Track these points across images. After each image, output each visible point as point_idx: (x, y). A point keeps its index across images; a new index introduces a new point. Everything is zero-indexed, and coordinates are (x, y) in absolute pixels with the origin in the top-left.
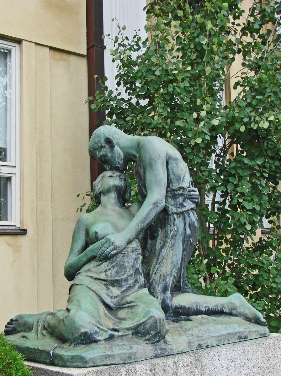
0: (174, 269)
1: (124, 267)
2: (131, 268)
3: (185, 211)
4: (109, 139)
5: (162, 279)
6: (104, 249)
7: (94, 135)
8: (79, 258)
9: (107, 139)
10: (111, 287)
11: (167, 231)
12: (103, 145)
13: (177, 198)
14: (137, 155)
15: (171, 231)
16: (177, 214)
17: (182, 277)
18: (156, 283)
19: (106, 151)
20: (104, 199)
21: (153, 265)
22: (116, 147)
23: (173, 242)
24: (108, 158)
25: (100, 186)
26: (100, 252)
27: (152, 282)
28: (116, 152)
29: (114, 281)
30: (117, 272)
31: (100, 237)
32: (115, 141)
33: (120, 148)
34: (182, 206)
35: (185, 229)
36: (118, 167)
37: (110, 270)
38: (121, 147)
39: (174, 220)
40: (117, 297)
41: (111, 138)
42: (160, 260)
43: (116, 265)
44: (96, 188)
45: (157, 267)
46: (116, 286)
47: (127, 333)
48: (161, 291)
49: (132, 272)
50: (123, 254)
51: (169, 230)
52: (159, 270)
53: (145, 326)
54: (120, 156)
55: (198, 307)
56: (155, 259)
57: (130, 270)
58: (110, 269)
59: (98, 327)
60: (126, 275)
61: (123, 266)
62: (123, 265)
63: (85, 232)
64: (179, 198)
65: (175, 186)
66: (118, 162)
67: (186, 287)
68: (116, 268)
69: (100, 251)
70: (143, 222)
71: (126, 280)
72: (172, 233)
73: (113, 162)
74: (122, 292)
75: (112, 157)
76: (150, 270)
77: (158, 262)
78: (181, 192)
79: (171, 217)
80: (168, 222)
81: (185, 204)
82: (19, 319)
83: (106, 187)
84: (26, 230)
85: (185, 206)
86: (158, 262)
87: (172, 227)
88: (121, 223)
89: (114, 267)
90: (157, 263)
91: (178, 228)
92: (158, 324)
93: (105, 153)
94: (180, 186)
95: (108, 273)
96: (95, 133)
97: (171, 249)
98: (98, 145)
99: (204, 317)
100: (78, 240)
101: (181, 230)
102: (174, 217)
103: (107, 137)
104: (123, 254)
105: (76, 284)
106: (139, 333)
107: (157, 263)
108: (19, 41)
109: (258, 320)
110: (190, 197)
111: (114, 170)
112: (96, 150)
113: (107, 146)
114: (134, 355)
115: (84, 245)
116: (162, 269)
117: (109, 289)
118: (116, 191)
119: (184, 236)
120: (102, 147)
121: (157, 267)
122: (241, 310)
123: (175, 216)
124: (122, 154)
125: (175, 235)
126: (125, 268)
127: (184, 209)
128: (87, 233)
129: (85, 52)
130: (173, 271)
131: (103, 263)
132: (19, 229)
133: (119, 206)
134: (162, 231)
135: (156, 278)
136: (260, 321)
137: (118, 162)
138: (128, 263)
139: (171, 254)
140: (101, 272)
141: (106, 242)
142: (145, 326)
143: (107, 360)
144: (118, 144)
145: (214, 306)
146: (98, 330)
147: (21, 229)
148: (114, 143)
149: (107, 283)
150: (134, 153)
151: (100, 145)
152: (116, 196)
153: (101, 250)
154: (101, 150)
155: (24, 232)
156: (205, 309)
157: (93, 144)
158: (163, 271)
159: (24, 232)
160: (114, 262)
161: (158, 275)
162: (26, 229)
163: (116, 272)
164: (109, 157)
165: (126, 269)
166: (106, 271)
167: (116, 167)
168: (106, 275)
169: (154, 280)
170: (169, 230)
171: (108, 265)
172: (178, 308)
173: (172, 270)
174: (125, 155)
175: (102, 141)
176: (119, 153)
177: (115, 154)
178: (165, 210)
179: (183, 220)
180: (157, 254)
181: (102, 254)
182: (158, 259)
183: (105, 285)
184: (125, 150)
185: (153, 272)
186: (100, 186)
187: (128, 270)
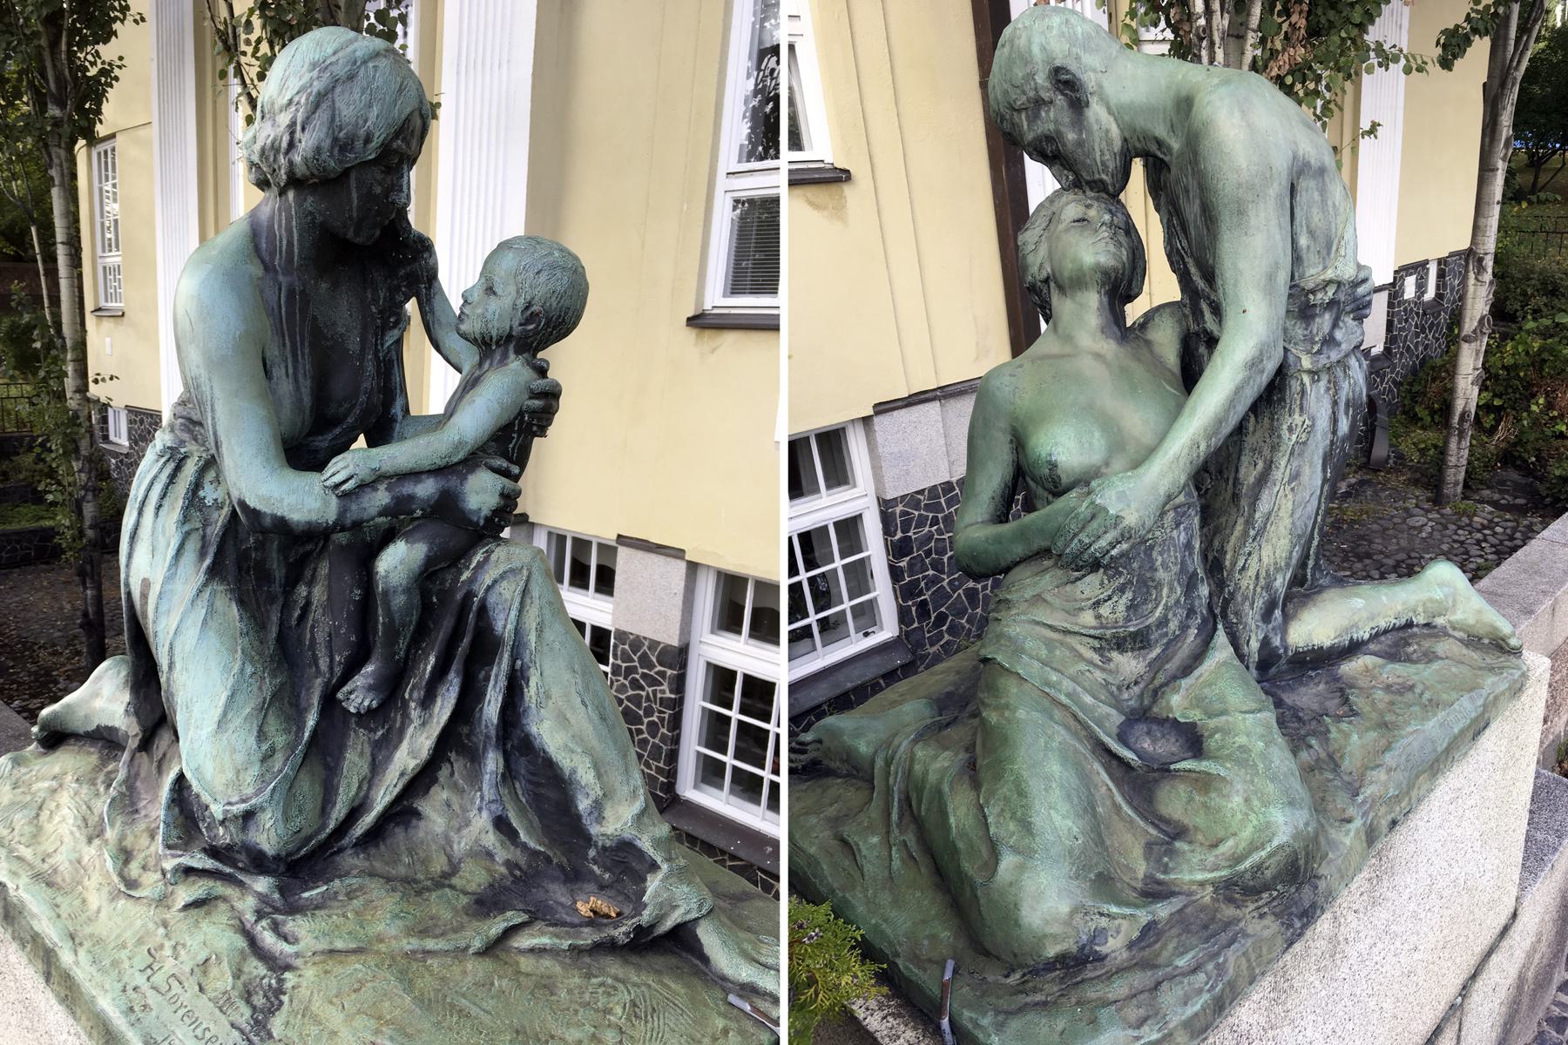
4: (1068, 72)
5: (1262, 582)
6: (1087, 541)
7: (1006, 50)
8: (998, 539)
9: (1057, 70)
10: (1115, 655)
11: (1279, 428)
12: (1045, 95)
13: (1313, 316)
14: (1175, 145)
15: (1290, 429)
17: (1312, 557)
18: (1245, 598)
19: (1056, 122)
20: (1063, 306)
21: (1233, 539)
22: (1093, 101)
23: (1295, 464)
24: (1064, 145)
25: (1043, 250)
26: (1075, 544)
27: (1232, 594)
28: (1096, 127)
29: (1124, 638)
30: (1132, 607)
31: (1065, 480)
32: (1089, 80)
34: (1330, 341)
35: (1335, 421)
36: (1102, 181)
38: (1112, 103)
39: (1303, 392)
40: (1136, 683)
41: (1073, 67)
44: (1030, 259)
45: (1247, 550)
46: (1133, 650)
48: (1258, 617)
51: (1285, 427)
52: (1255, 557)
54: (1110, 143)
56: (1241, 521)
57: (1171, 589)
58: (1110, 598)
60: (1160, 608)
63: (1009, 438)
64: (1321, 315)
66: (1103, 163)
68: (1129, 595)
70: (1215, 433)
72: (1294, 437)
73: (1084, 163)
74: (1150, 665)
75: (1080, 143)
76: (1223, 552)
77: (1252, 533)
78: (1330, 294)
79: (1293, 382)
80: (1283, 399)
82: (825, 739)
86: (1252, 533)
87: (1296, 416)
88: (1138, 419)
89: (1122, 590)
90: (1245, 534)
91: (1313, 419)
92: (1302, 862)
93: (1052, 127)
94: (1330, 274)
95: (1105, 610)
97: (1288, 488)
98: (1024, 93)
100: (990, 464)
101: (1323, 423)
102: (1302, 384)
103: (1058, 63)
107: (1245, 534)
108: (700, 322)
112: (1019, 111)
113: (1060, 100)
115: (1009, 478)
116: (1264, 553)
117: (1110, 660)
118: (1103, 285)
120: (1039, 103)
121: (1247, 550)
124: (1115, 131)
125: (1304, 443)
128: (1019, 443)
133: (1116, 339)
135: (1244, 583)
137: (1103, 163)
138: (1165, 566)
139: (1290, 505)
140: (1081, 609)
141: (1093, 517)
150: (1161, 131)
151: (1032, 94)
152: (1105, 299)
154: (1037, 116)
157: (1006, 86)
158: (1265, 560)
160: (1121, 574)
161: (1251, 572)
163: (1128, 608)
164: (1070, 146)
166: (1097, 604)
167: (1095, 182)
168: (1099, 617)
169: (1238, 587)
170: (1285, 427)
171: (1102, 584)
174: (1127, 135)
175: (1041, 79)
176: (1107, 131)
177: (1090, 133)
179: (1328, 389)
180: (1244, 503)
182: (1249, 522)
183: (1095, 649)
184: (1127, 118)
185: (1234, 564)
186: (1043, 250)
187: (1165, 591)
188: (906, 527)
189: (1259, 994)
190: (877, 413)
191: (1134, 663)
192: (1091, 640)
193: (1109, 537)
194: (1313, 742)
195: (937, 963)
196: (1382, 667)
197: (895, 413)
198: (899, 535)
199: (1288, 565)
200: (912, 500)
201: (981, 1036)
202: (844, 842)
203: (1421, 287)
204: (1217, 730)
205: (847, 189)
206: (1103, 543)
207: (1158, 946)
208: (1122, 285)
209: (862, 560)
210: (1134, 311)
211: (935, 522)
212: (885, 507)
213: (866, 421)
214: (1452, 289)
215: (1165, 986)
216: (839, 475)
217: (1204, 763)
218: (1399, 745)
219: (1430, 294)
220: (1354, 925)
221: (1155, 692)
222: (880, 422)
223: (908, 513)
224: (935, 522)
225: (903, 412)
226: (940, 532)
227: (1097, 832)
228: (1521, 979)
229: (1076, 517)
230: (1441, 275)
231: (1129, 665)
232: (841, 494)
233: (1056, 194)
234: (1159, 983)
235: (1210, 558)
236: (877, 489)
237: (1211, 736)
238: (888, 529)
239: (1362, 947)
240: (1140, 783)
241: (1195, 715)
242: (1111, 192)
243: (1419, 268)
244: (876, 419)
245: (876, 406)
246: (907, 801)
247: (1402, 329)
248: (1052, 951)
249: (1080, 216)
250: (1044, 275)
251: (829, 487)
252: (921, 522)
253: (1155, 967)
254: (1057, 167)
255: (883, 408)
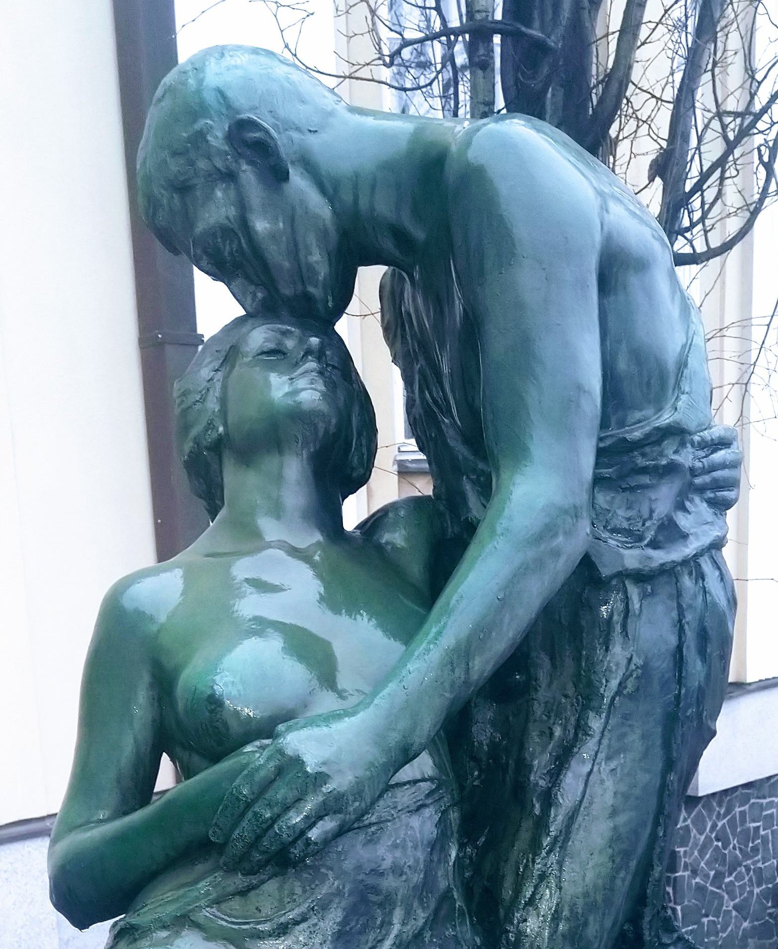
0: (622, 874)
1: (380, 898)
2: (416, 904)
3: (685, 562)
4: (251, 124)
16: (641, 577)
20: (236, 480)
32: (284, 142)
33: (322, 189)
34: (669, 532)
42: (553, 830)
43: (339, 893)
49: (421, 922)
61: (373, 898)
62: (376, 890)
65: (640, 425)
69: (245, 823)
81: (684, 521)
83: (245, 412)
85: (685, 536)
89: (324, 907)
96: (170, 89)
103: (244, 116)
104: (371, 825)
111: (284, 313)
126: (381, 905)
128: (164, 682)
129: (666, 138)
130: (619, 882)
131: (263, 882)
134: (554, 666)
148: (283, 151)
153: (250, 815)
165: (391, 913)
173: (613, 879)
178: (588, 576)
182: (542, 824)
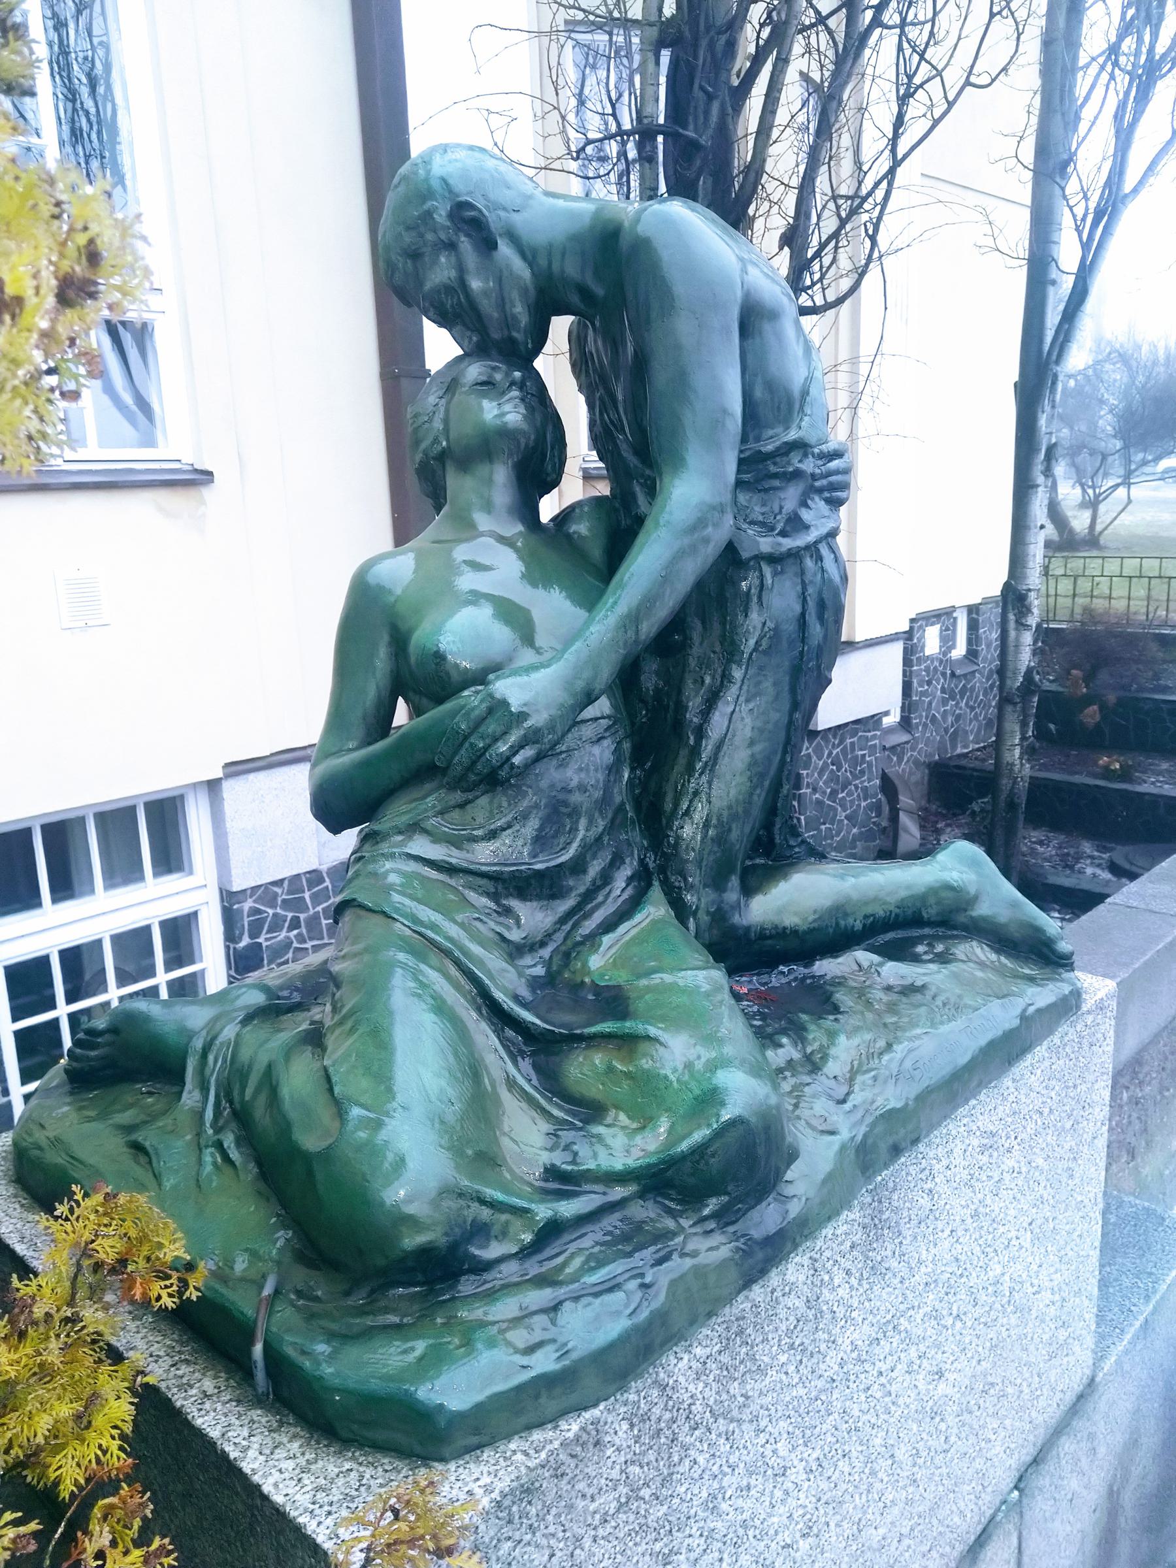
0: (758, 791)
2: (597, 815)
3: (807, 548)
4: (471, 206)
8: (366, 763)
20: (456, 483)
31: (455, 677)
34: (795, 524)
37: (509, 831)
43: (536, 806)
47: (618, 1192)
49: (601, 829)
50: (561, 752)
53: (702, 1165)
55: (842, 923)
59: (482, 1201)
60: (575, 845)
62: (565, 803)
67: (792, 843)
69: (463, 752)
71: (577, 866)
74: (563, 920)
81: (806, 515)
83: (463, 430)
84: (210, 474)
85: (807, 527)
89: (525, 816)
96: (405, 178)
99: (865, 964)
103: (462, 199)
104: (561, 752)
105: (362, 906)
106: (673, 1187)
109: (1045, 950)
110: (824, 482)
111: (494, 352)
114: (663, 1324)
119: (796, 653)
122: (983, 909)
123: (767, 570)
126: (569, 815)
127: (800, 541)
128: (399, 641)
131: (477, 797)
132: (190, 468)
136: (1054, 951)
142: (702, 1165)
143: (543, 1400)
144: (513, 238)
145: (892, 908)
146: (485, 1213)
147: (196, 470)
148: (493, 226)
149: (500, 887)
153: (467, 745)
155: (201, 478)
156: (864, 925)
159: (201, 478)
162: (210, 469)
165: (577, 822)
169: (678, 838)
172: (771, 937)
178: (731, 559)
181: (474, 763)
182: (695, 752)
185: (676, 805)
187: (583, 823)
188: (255, 932)
189: (705, 1344)
190: (228, 776)
191: (540, 916)
192: (483, 882)
193: (513, 738)
194: (785, 1040)
195: (253, 1282)
196: (881, 965)
197: (252, 776)
198: (245, 941)
199: (747, 812)
200: (266, 893)
201: (307, 1364)
202: (138, 1148)
203: (948, 640)
204: (649, 989)
205: (207, 492)
206: (503, 748)
207: (560, 1260)
208: (538, 465)
209: (193, 975)
210: (549, 507)
211: (295, 923)
212: (229, 900)
213: (213, 786)
214: (988, 646)
215: (568, 1305)
216: (170, 857)
217: (628, 1024)
218: (900, 1049)
219: (960, 650)
220: (843, 1292)
221: (567, 955)
222: (232, 790)
223: (259, 911)
224: (295, 923)
225: (262, 775)
226: (301, 939)
227: (480, 1107)
228: (1113, 1495)
229: (468, 714)
230: (973, 626)
231: (533, 917)
232: (172, 882)
233: (458, 360)
234: (561, 1303)
235: (645, 804)
236: (220, 878)
237: (640, 997)
238: (230, 936)
239: (860, 1334)
240: (542, 1048)
241: (620, 977)
242: (519, 352)
243: (943, 616)
244: (227, 785)
245: (227, 765)
246: (226, 1092)
247: (923, 694)
248: (412, 1241)
249: (484, 378)
250: (437, 449)
251: (156, 874)
252: (275, 926)
253: (554, 1283)
254: (459, 327)
255: (238, 768)
